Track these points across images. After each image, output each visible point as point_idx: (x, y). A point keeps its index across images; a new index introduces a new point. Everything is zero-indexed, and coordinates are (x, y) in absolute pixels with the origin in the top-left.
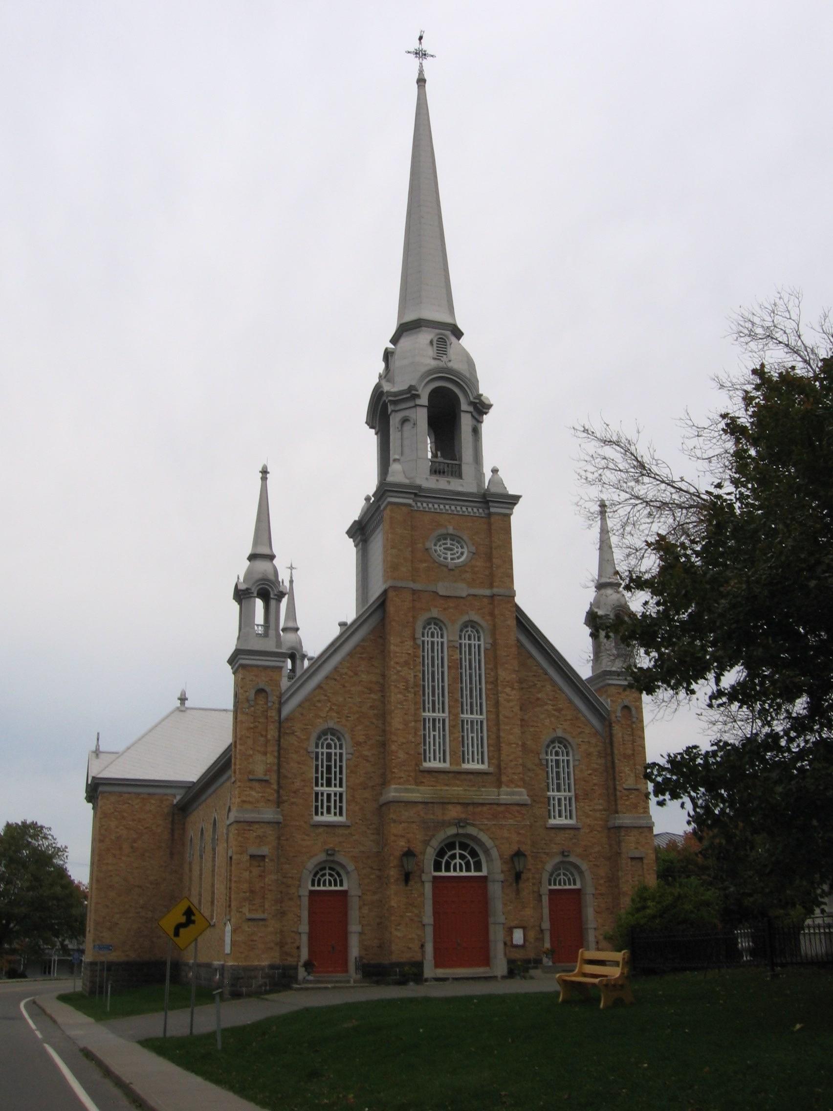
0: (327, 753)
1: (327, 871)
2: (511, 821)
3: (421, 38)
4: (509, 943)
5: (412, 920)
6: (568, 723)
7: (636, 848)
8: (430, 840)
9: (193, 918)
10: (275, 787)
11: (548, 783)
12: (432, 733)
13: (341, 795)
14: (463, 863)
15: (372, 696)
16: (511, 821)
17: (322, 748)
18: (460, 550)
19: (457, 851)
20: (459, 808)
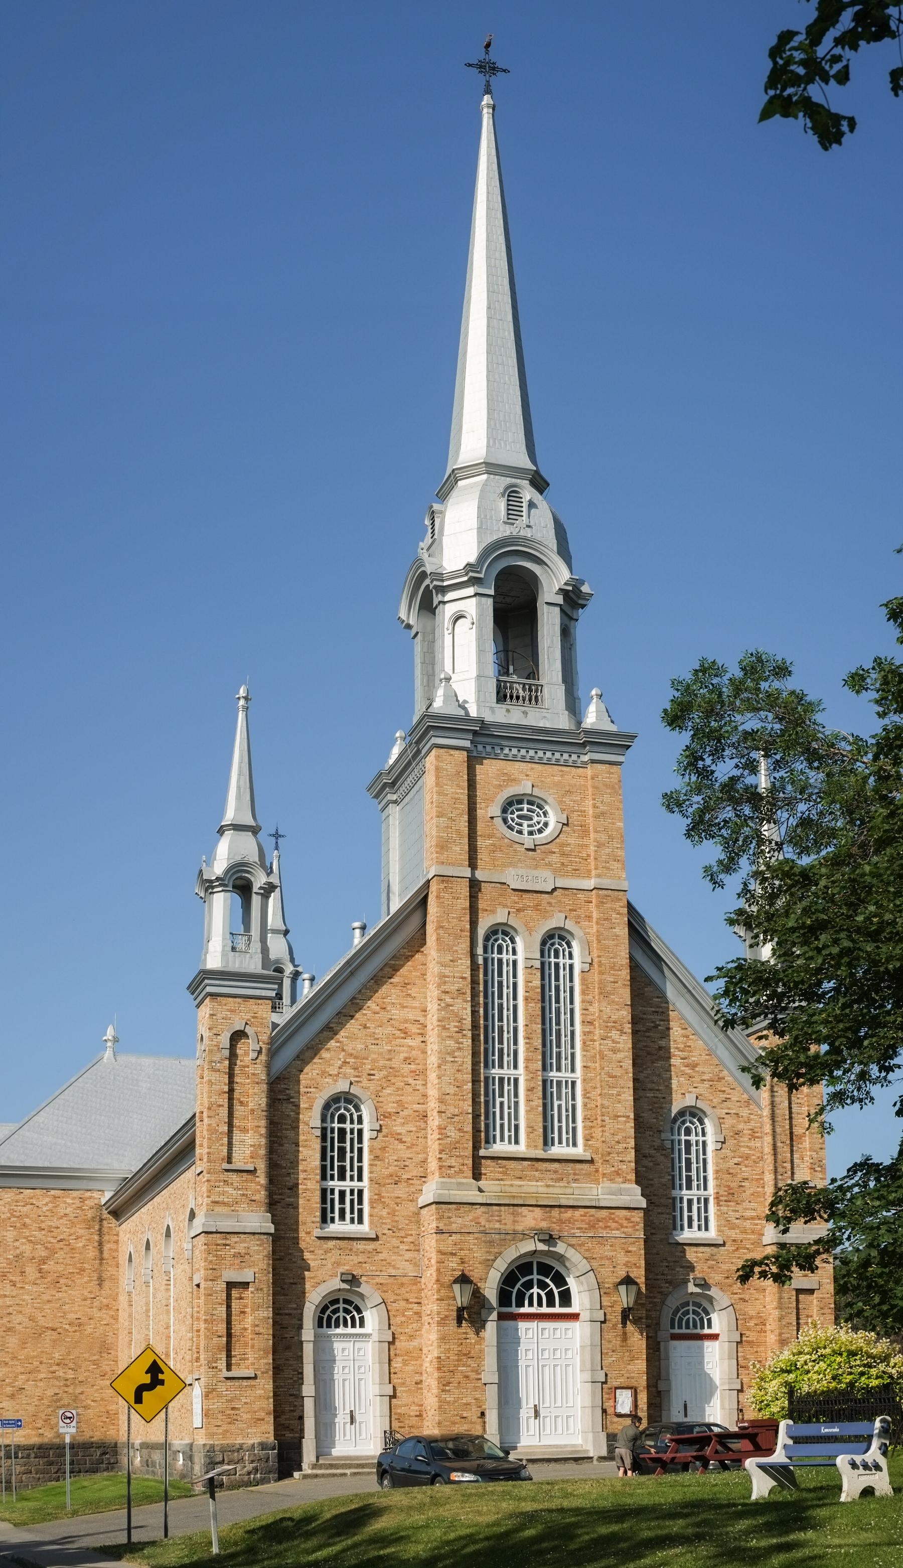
0: (339, 1129)
1: (691, 1308)
2: (617, 1233)
3: (488, 46)
4: (610, 1411)
5: (467, 1377)
6: (707, 1085)
8: (494, 1261)
9: (161, 1376)
11: (673, 1176)
12: (498, 1100)
13: (360, 1192)
14: (543, 1294)
15: (409, 1041)
16: (617, 1233)
18: (543, 819)
19: (535, 1277)
20: (538, 1211)
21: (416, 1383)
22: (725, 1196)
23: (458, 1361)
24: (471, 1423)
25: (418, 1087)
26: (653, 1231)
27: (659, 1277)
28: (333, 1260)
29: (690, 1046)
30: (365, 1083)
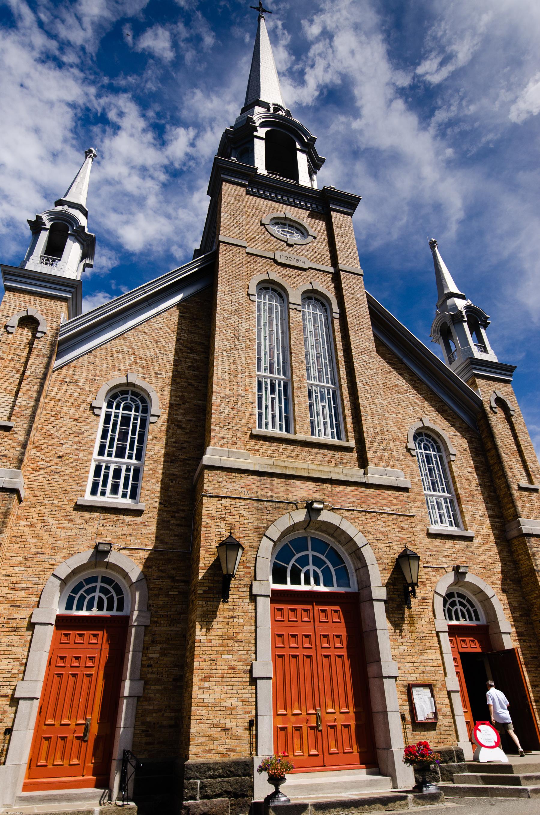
5: (232, 668)
8: (267, 528)
14: (319, 571)
17: (118, 408)
20: (311, 485)
21: (174, 680)
22: (466, 496)
23: (222, 645)
24: (237, 737)
25: (200, 388)
28: (94, 530)
30: (152, 379)
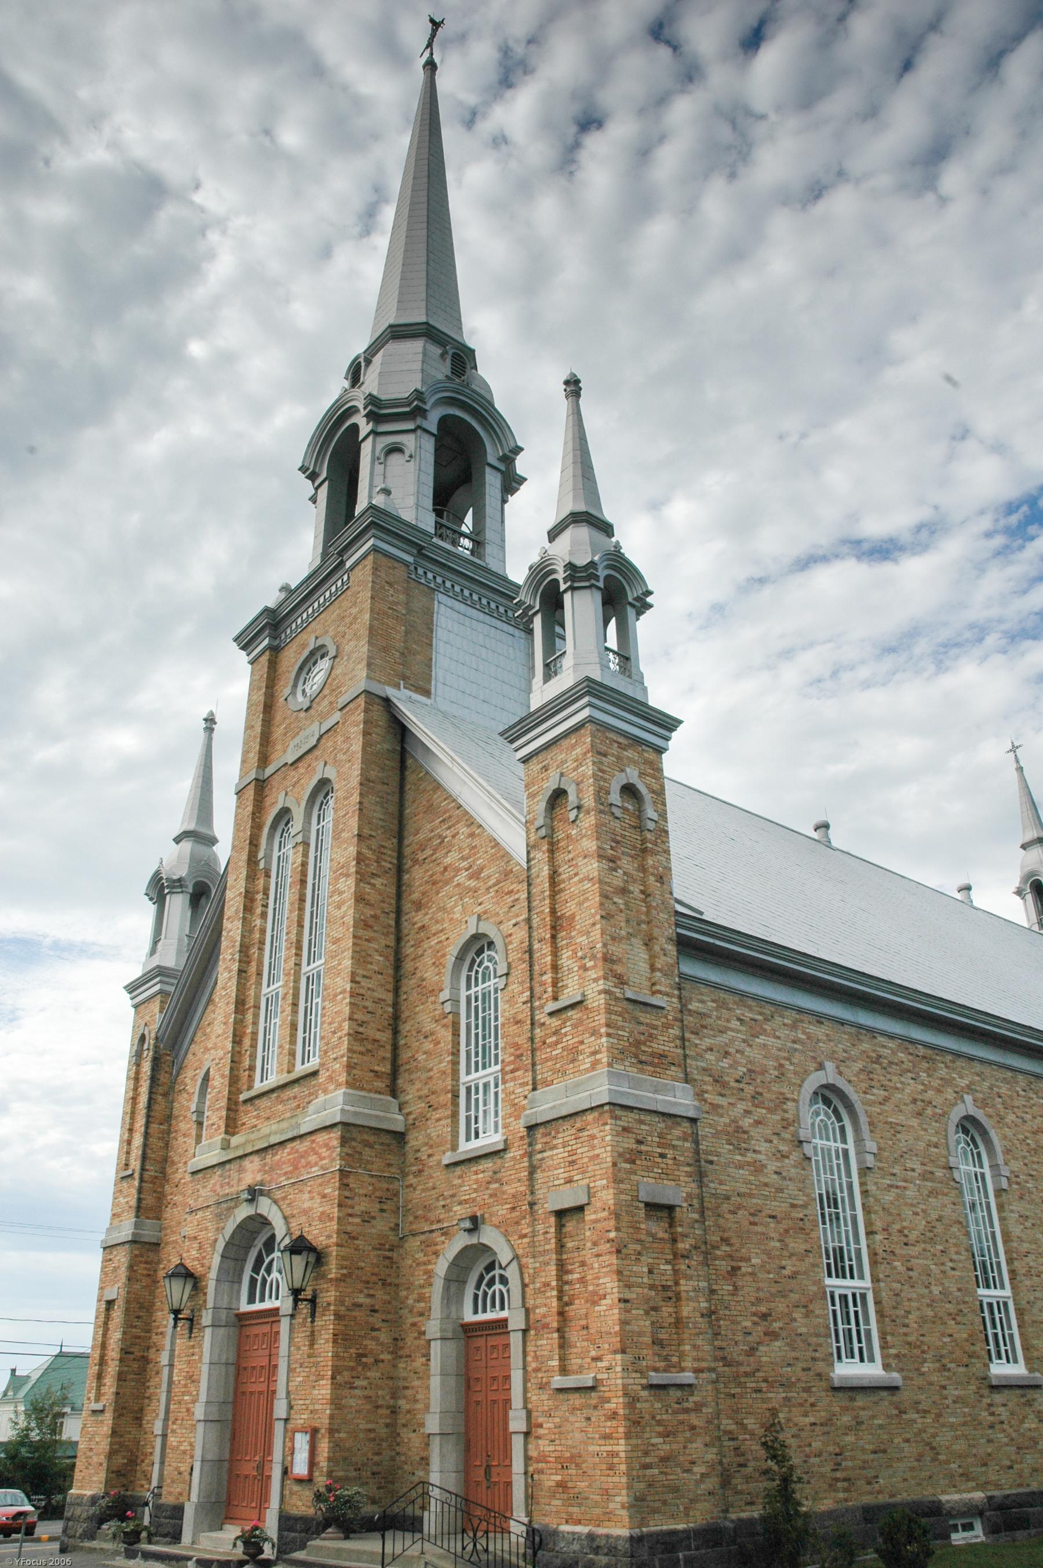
7: (569, 1181)
10: (136, 1183)
26: (430, 1151)
27: (434, 1227)
29: (475, 847)
